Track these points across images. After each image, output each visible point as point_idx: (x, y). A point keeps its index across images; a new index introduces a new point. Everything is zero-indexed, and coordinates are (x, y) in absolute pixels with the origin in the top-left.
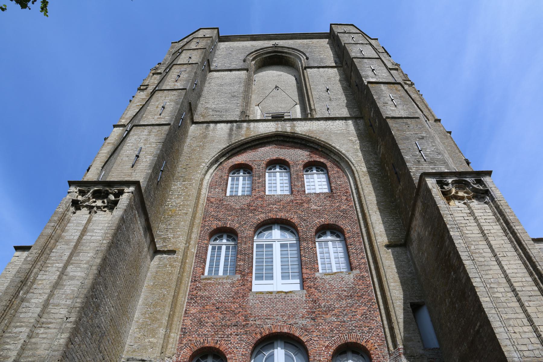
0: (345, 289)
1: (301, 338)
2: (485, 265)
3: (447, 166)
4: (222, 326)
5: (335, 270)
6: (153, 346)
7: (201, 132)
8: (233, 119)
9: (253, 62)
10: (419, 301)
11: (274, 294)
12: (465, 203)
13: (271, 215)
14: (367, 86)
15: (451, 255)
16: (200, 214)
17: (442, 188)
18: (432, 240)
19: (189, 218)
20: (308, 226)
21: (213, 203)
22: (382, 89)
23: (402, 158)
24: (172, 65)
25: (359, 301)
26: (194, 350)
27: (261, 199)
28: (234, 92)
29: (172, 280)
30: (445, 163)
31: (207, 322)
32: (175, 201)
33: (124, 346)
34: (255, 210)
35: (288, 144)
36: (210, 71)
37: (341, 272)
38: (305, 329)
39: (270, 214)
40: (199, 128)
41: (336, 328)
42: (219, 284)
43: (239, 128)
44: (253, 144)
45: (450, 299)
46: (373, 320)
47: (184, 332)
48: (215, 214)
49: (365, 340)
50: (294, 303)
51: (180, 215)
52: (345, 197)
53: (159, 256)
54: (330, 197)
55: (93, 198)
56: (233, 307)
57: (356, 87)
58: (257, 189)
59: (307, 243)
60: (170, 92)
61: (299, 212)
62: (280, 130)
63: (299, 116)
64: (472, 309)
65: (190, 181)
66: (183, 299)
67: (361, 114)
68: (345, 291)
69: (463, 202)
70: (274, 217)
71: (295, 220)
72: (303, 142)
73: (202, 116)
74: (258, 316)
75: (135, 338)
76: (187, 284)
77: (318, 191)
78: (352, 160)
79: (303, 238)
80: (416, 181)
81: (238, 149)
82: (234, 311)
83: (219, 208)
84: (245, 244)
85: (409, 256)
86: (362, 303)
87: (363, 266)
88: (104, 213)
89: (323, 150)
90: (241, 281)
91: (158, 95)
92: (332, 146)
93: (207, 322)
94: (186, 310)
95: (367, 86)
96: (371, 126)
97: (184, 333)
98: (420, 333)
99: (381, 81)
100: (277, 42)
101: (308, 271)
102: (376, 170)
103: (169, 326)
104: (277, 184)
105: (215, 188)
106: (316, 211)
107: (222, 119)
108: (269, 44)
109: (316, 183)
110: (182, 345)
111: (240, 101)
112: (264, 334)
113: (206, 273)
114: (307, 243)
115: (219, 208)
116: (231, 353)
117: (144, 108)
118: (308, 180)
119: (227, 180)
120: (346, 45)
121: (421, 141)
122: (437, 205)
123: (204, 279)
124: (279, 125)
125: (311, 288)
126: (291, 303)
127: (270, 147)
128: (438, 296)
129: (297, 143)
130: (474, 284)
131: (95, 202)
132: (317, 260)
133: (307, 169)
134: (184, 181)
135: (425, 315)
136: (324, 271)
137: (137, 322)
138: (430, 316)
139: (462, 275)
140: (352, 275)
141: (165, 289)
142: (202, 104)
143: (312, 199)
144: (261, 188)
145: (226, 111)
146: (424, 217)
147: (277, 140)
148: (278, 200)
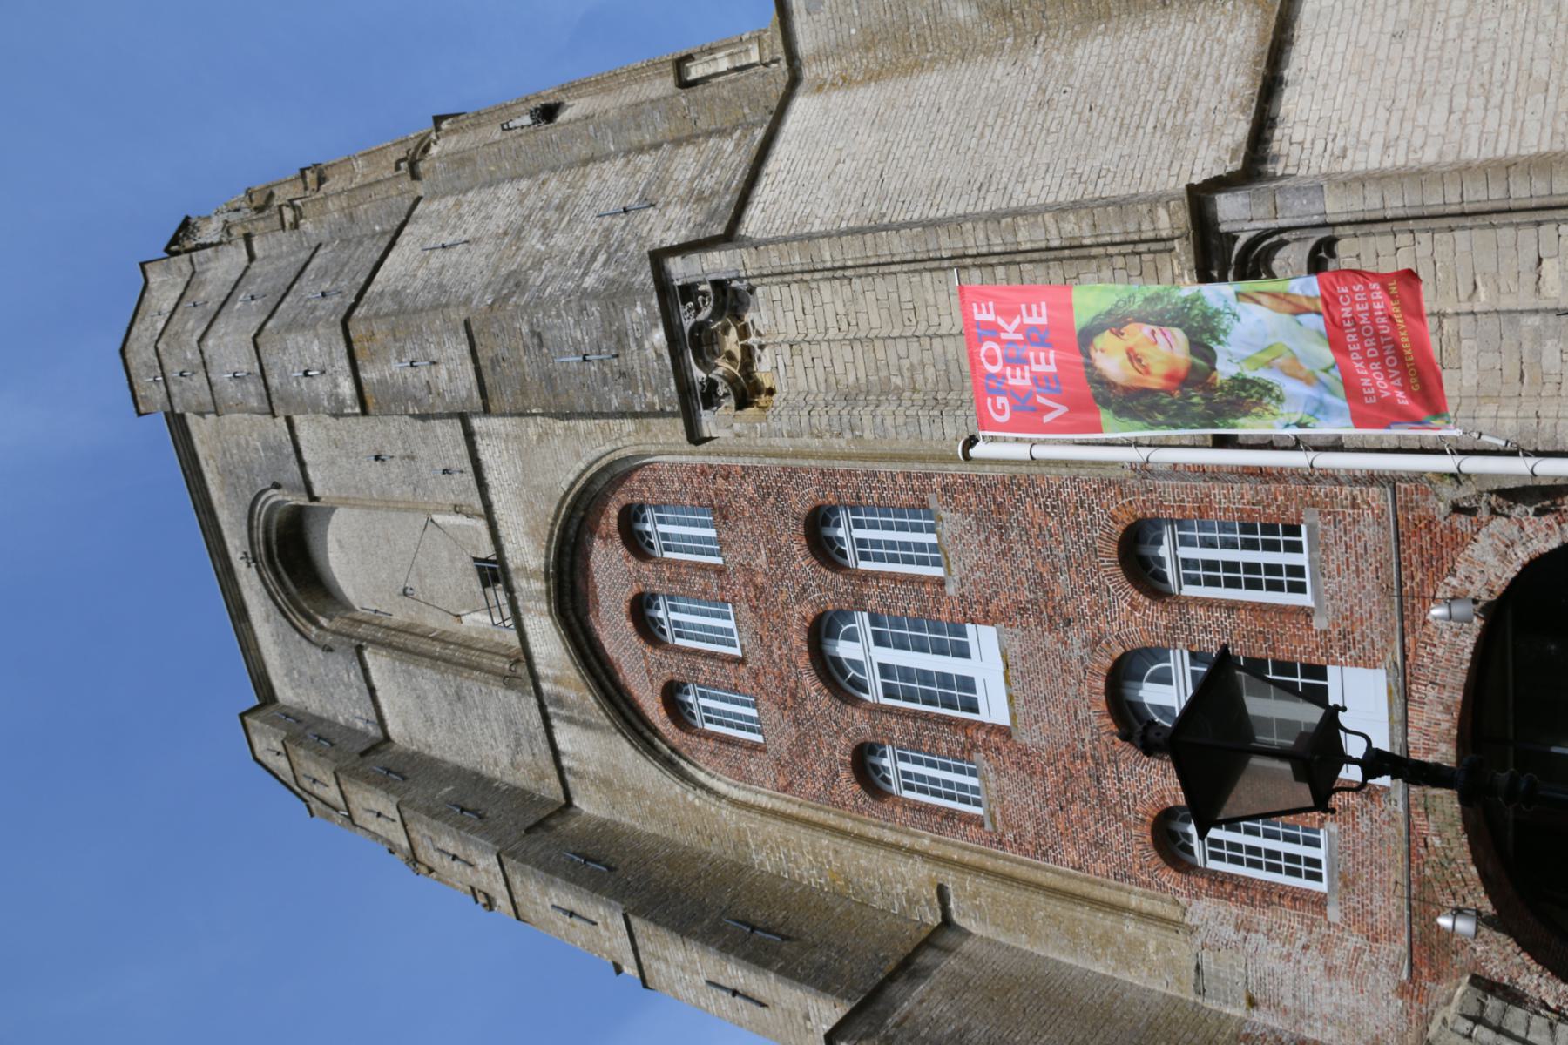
2: (947, 371)
9: (323, 621)
13: (803, 661)
25: (1011, 514)
26: (1162, 864)
31: (1097, 832)
33: (1171, 998)
35: (580, 583)
36: (387, 739)
38: (1094, 643)
39: (800, 664)
41: (1086, 580)
43: (559, 701)
44: (599, 670)
50: (1031, 654)
53: (955, 917)
54: (725, 517)
56: (1053, 777)
69: (758, 351)
72: (568, 549)
74: (1072, 733)
78: (604, 449)
81: (624, 707)
82: (1065, 779)
89: (582, 506)
93: (1097, 832)
97: (1126, 876)
100: (239, 565)
103: (1118, 909)
108: (250, 582)
116: (1163, 797)
126: (1031, 661)
127: (598, 627)
129: (573, 565)
137: (1115, 970)
140: (943, 514)
147: (574, 609)
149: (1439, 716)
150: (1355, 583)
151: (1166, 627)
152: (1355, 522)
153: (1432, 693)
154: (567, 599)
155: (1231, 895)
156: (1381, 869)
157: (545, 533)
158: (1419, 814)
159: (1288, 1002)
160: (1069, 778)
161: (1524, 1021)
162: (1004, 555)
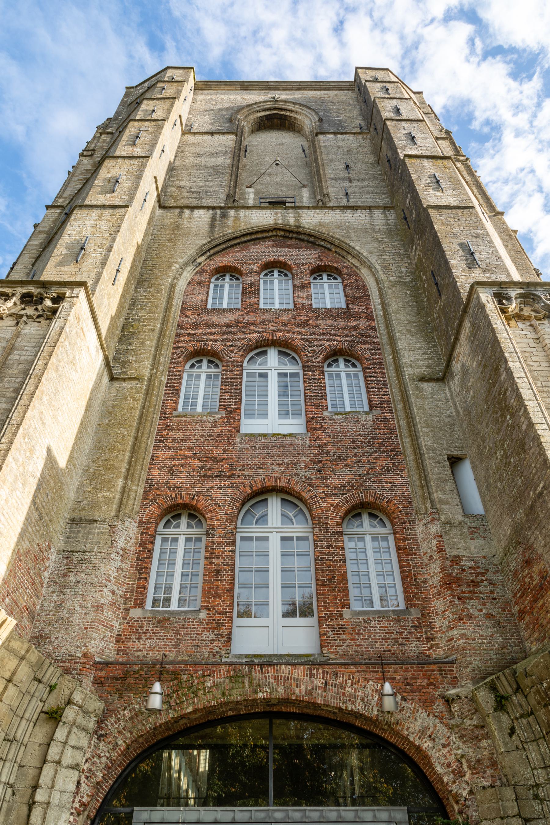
0: (362, 433)
1: (303, 494)
3: (509, 275)
4: (201, 476)
5: (348, 408)
6: (108, 501)
7: (172, 220)
8: (215, 204)
10: (460, 453)
11: (268, 437)
12: (531, 325)
13: (267, 335)
14: (404, 160)
15: (508, 393)
16: (171, 331)
17: (500, 303)
18: (482, 373)
19: (155, 336)
20: (314, 350)
21: (189, 318)
22: (423, 166)
23: (447, 263)
24: (127, 121)
27: (253, 314)
28: (217, 166)
29: (133, 416)
30: (506, 271)
32: (137, 314)
34: (245, 327)
37: (356, 412)
39: (264, 334)
40: (169, 215)
41: (348, 483)
42: (197, 423)
43: (224, 216)
45: (502, 452)
46: (398, 474)
47: (150, 484)
48: (193, 332)
49: (386, 500)
50: (295, 449)
51: (145, 332)
52: (365, 315)
55: (21, 303)
57: (388, 163)
58: (248, 301)
59: (314, 373)
60: (128, 162)
61: (304, 332)
62: (280, 221)
63: (306, 203)
64: (533, 465)
65: (158, 287)
66: (149, 442)
67: (392, 202)
68: (361, 436)
70: (270, 338)
71: (298, 342)
72: (312, 239)
73: (173, 198)
75: (85, 492)
76: (155, 422)
77: (328, 306)
79: (308, 366)
80: (464, 294)
81: (223, 246)
82: (216, 458)
83: (197, 324)
84: (232, 371)
85: (448, 395)
86: (383, 452)
87: (385, 405)
88: (37, 324)
89: (338, 250)
90: (226, 419)
91: (108, 163)
92: (350, 246)
94: (153, 456)
95: (404, 160)
96: (405, 218)
97: (151, 486)
98: (459, 495)
99: (424, 154)
101: (314, 409)
102: (408, 280)
104: (276, 294)
105: (192, 298)
106: (324, 332)
107: (200, 204)
109: (328, 295)
110: (148, 501)
111: (227, 177)
112: (255, 488)
113: (180, 409)
114: (314, 373)
115: (197, 324)
117: (90, 182)
118: (316, 291)
119: (208, 288)
120: (377, 101)
121: (475, 240)
122: (492, 326)
123: (176, 416)
124: (279, 215)
125: (317, 430)
128: (485, 447)
130: (539, 432)
131: (24, 309)
132: (326, 395)
133: (315, 275)
134: (149, 287)
135: (467, 471)
136: (335, 410)
138: (474, 473)
139: (522, 419)
141: (125, 428)
142: (173, 181)
143: (321, 316)
144: (253, 300)
145: (206, 193)
146: (472, 342)
148: (276, 316)
149: (303, 687)
150: (377, 637)
151: (327, 524)
152: (418, 639)
153: (319, 682)
154: (282, 233)
155: (145, 548)
156: (176, 646)
157: (323, 230)
158: (228, 671)
159: (72, 578)
160: (216, 461)
161: (80, 745)
162: (354, 442)
